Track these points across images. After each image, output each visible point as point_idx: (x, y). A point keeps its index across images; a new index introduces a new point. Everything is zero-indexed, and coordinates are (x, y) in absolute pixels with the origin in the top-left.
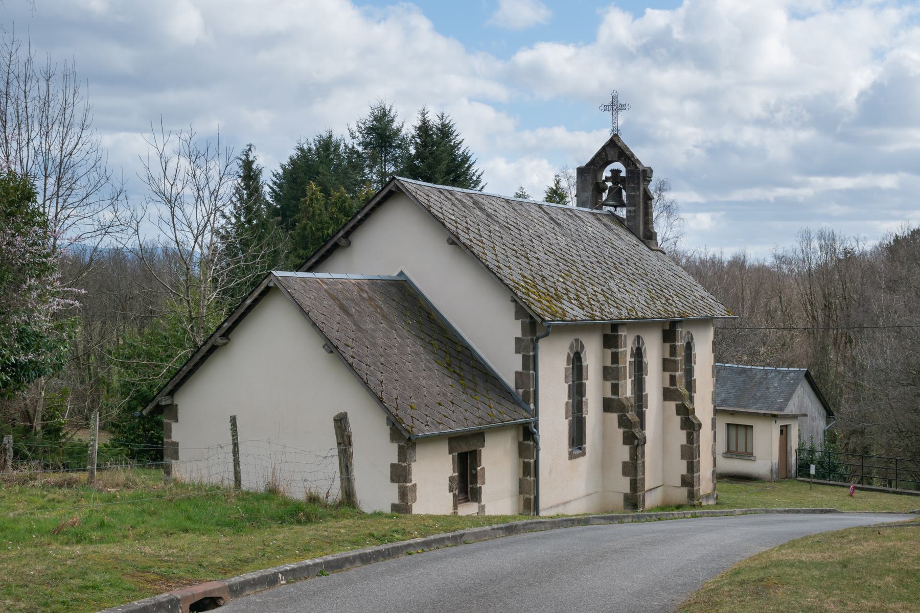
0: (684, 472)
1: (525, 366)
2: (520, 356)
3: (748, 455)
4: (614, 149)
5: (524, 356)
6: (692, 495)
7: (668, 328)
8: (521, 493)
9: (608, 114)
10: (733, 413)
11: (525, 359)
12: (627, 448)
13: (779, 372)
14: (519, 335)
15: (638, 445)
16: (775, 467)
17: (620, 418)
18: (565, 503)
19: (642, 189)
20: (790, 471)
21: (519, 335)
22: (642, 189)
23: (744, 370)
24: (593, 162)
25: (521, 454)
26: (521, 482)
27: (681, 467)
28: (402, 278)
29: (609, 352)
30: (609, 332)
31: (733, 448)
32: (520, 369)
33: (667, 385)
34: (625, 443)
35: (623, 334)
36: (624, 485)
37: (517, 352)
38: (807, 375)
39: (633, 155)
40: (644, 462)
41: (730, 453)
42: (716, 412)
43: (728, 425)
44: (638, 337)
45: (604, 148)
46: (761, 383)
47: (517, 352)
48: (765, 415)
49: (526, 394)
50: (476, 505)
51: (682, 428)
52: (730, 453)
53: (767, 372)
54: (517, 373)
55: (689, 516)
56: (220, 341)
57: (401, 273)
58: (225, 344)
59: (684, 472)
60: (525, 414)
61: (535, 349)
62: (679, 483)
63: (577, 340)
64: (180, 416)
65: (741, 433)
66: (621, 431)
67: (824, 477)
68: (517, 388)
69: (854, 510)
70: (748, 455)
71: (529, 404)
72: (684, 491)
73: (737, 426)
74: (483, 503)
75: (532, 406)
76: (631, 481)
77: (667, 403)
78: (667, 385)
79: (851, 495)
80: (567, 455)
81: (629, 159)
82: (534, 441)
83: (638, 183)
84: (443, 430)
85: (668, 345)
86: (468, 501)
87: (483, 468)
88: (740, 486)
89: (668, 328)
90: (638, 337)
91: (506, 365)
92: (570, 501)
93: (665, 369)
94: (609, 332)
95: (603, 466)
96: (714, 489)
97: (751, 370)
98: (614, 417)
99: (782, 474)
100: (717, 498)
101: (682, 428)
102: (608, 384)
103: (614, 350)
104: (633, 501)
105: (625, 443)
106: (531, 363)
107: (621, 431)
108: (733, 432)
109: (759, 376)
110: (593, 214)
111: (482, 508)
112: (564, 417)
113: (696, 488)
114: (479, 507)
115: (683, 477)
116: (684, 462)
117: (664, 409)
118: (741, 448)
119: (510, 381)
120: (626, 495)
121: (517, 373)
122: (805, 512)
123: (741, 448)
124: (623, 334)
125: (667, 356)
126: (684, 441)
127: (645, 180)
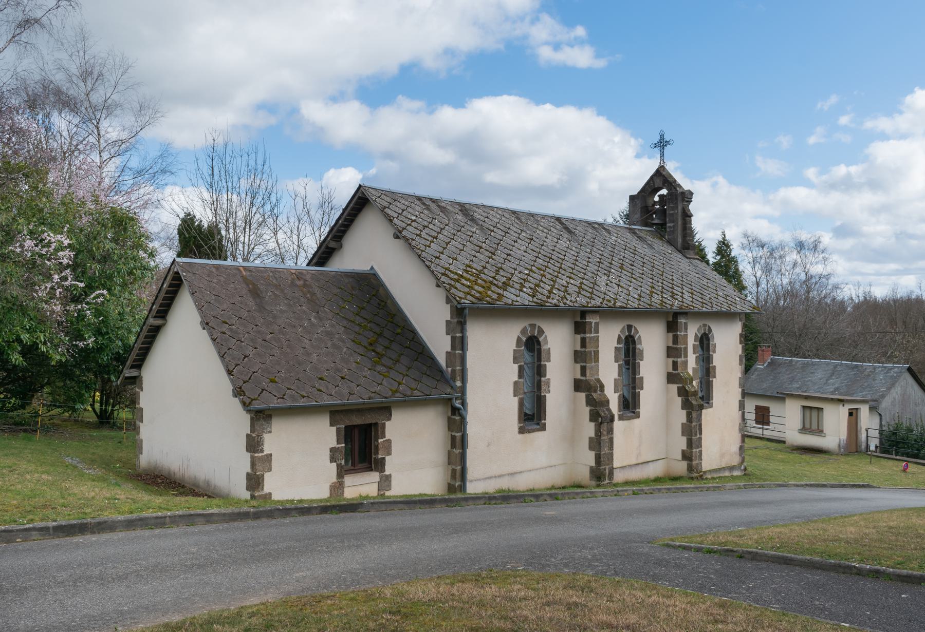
0: (685, 448)
1: (453, 347)
2: (449, 337)
3: (819, 432)
4: (661, 178)
5: (452, 337)
6: (690, 468)
7: (671, 319)
8: (449, 464)
9: (657, 150)
10: (807, 398)
11: (453, 339)
12: (593, 424)
13: (885, 367)
14: (449, 318)
15: (601, 423)
16: (843, 442)
17: (587, 397)
18: (512, 474)
19: (680, 208)
20: (860, 446)
21: (449, 318)
22: (680, 208)
23: (857, 366)
24: (643, 190)
25: (450, 429)
26: (449, 453)
27: (682, 443)
28: (372, 272)
29: (579, 337)
30: (578, 319)
31: (807, 426)
32: (449, 349)
33: (671, 370)
34: (591, 420)
35: (594, 321)
36: (590, 458)
37: (447, 334)
38: (910, 370)
39: (675, 181)
40: (611, 440)
41: (804, 430)
42: (744, 394)
43: (804, 407)
44: (630, 327)
45: (652, 178)
46: (869, 376)
47: (447, 334)
48: (832, 399)
49: (454, 371)
50: (374, 476)
51: (682, 408)
52: (804, 430)
53: (875, 368)
54: (447, 352)
55: (631, 492)
56: (158, 322)
57: (372, 268)
58: (164, 325)
59: (685, 448)
60: (449, 390)
61: (463, 331)
62: (680, 457)
63: (533, 326)
64: (144, 386)
65: (814, 413)
66: (588, 409)
67: (887, 452)
68: (447, 367)
69: (896, 486)
70: (819, 432)
71: (454, 380)
72: (684, 464)
73: (811, 408)
74: (387, 473)
75: (459, 384)
76: (596, 455)
77: (670, 385)
78: (671, 370)
79: (905, 470)
80: (517, 430)
81: (671, 184)
82: (460, 415)
83: (676, 203)
84: (327, 401)
85: (671, 335)
86: (372, 470)
87: (389, 441)
88: (807, 457)
89: (671, 319)
90: (630, 327)
91: (439, 345)
92: (521, 472)
93: (668, 356)
94: (578, 319)
95: (571, 439)
96: (743, 461)
97: (862, 366)
98: (582, 396)
99: (854, 447)
100: (745, 469)
101: (682, 408)
102: (578, 366)
103: (583, 335)
104: (601, 472)
105: (591, 420)
106: (459, 344)
107: (588, 409)
108: (808, 412)
109: (868, 370)
110: (630, 229)
111: (386, 482)
112: (512, 394)
113: (694, 463)
114: (381, 478)
115: (683, 452)
116: (685, 439)
117: (667, 391)
118: (814, 427)
119: (442, 360)
120: (591, 468)
121: (447, 352)
122: (832, 486)
123: (814, 427)
124: (594, 321)
125: (671, 344)
126: (684, 419)
127: (683, 200)
